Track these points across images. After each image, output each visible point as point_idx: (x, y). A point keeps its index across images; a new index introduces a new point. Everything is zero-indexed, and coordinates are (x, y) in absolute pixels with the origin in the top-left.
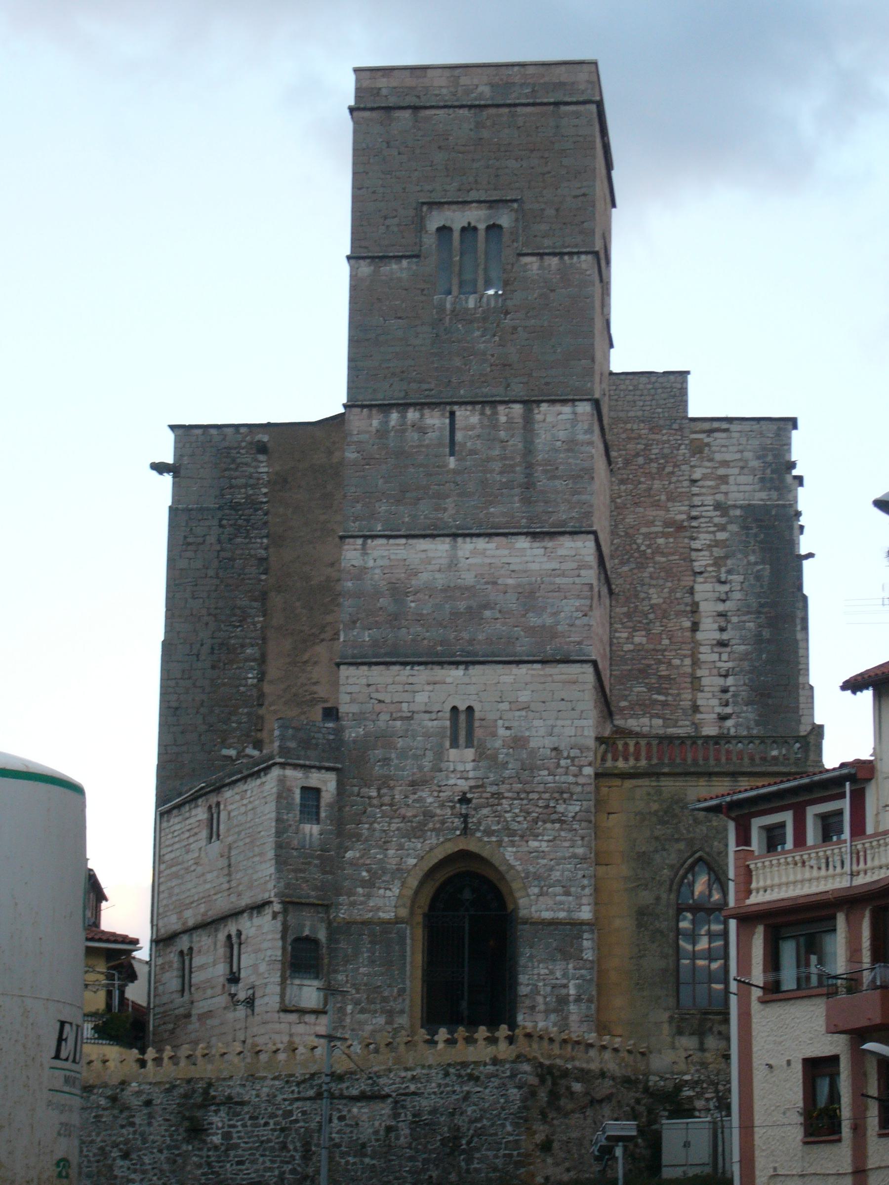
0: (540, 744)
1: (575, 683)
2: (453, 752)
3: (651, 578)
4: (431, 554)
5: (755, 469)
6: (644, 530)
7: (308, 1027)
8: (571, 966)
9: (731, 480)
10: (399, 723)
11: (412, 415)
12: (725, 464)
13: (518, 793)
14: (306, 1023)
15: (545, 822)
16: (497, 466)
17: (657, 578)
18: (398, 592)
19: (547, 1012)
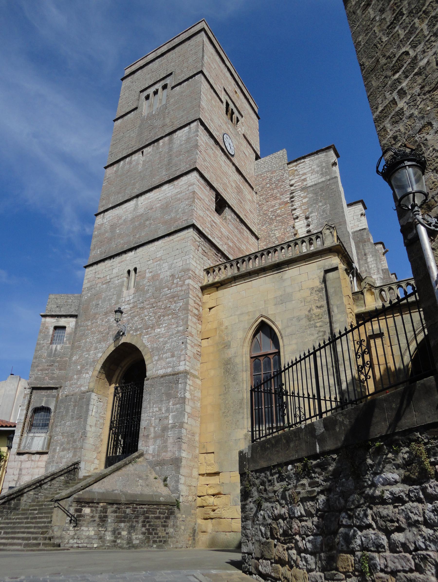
3: (275, 227)
5: (318, 171)
6: (271, 210)
7: (33, 463)
8: (171, 403)
9: (308, 179)
10: (105, 286)
12: (304, 174)
13: (152, 304)
14: (32, 460)
15: (164, 316)
17: (278, 226)
19: (155, 438)
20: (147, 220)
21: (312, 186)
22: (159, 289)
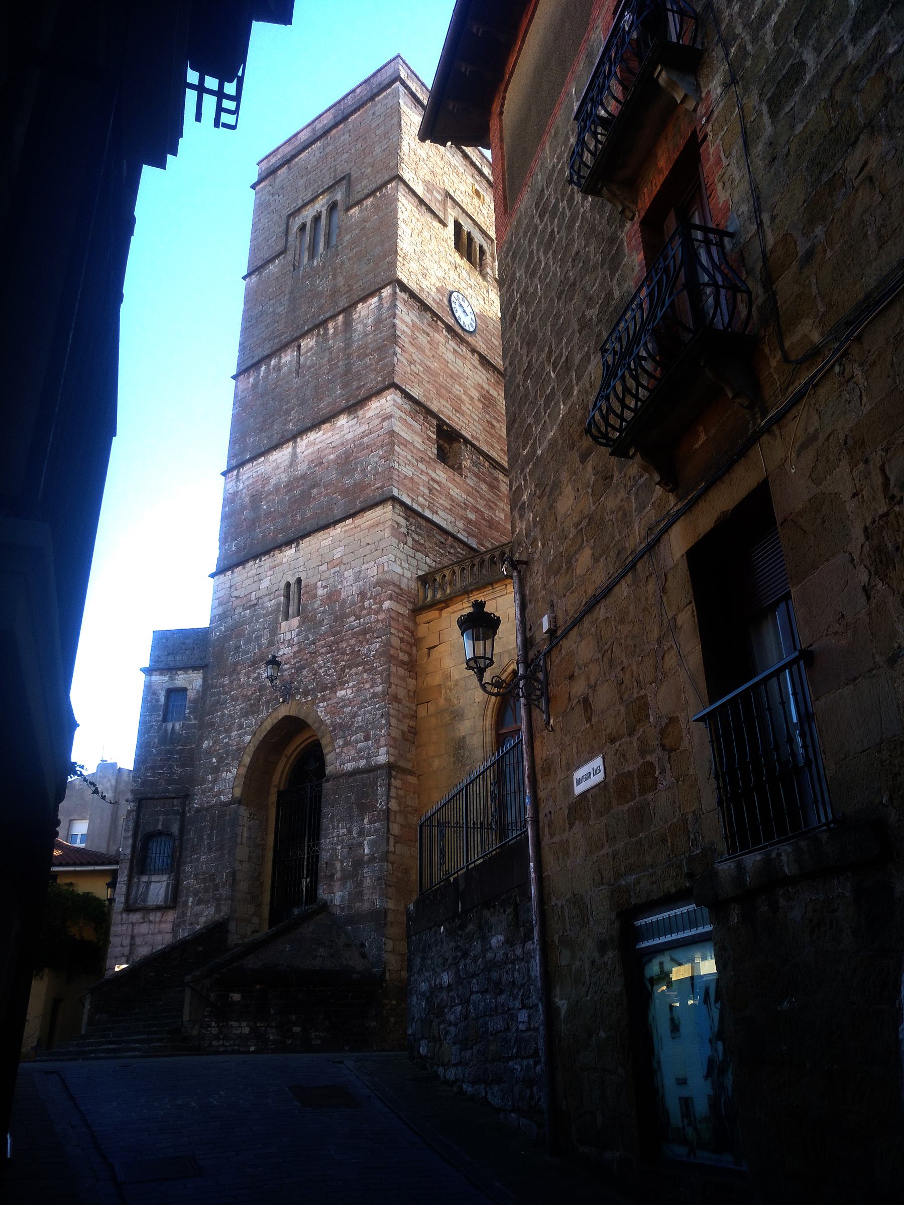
0: (350, 593)
1: (377, 525)
2: (284, 624)
4: (279, 461)
14: (150, 922)
15: (350, 668)
19: (344, 879)
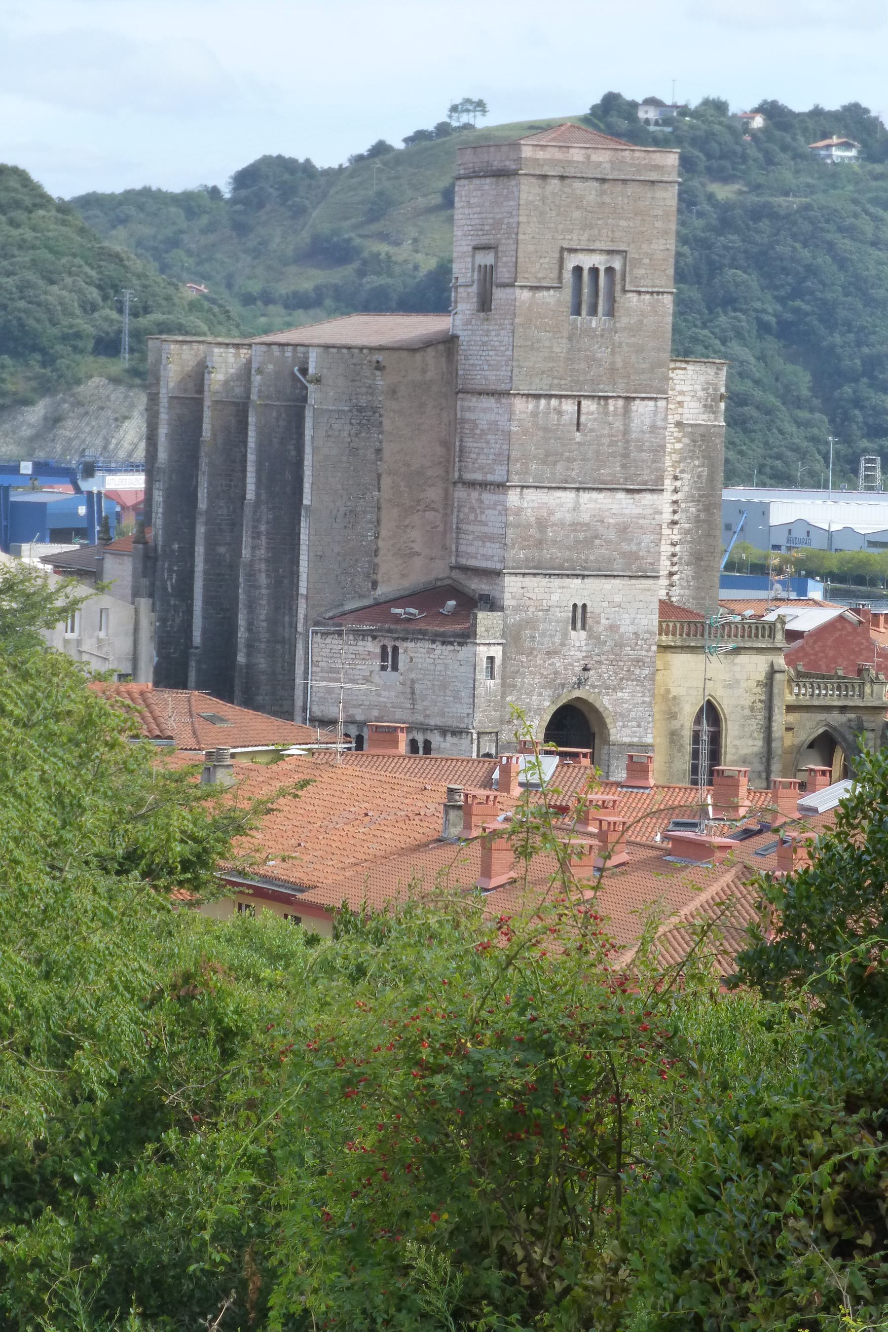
11: (554, 402)
16: (606, 441)
18: (542, 524)
20: (596, 537)
21: (691, 425)
22: (619, 645)
